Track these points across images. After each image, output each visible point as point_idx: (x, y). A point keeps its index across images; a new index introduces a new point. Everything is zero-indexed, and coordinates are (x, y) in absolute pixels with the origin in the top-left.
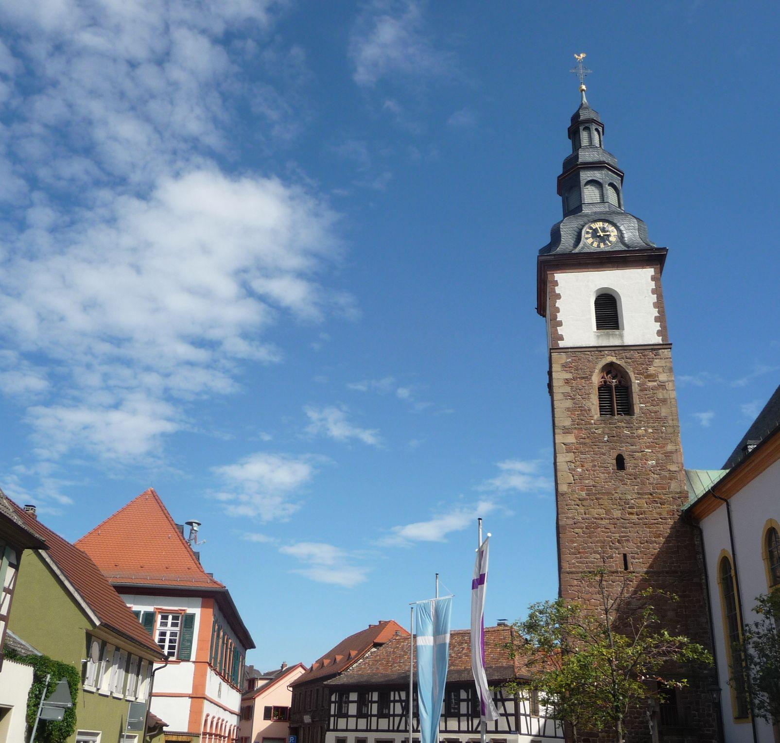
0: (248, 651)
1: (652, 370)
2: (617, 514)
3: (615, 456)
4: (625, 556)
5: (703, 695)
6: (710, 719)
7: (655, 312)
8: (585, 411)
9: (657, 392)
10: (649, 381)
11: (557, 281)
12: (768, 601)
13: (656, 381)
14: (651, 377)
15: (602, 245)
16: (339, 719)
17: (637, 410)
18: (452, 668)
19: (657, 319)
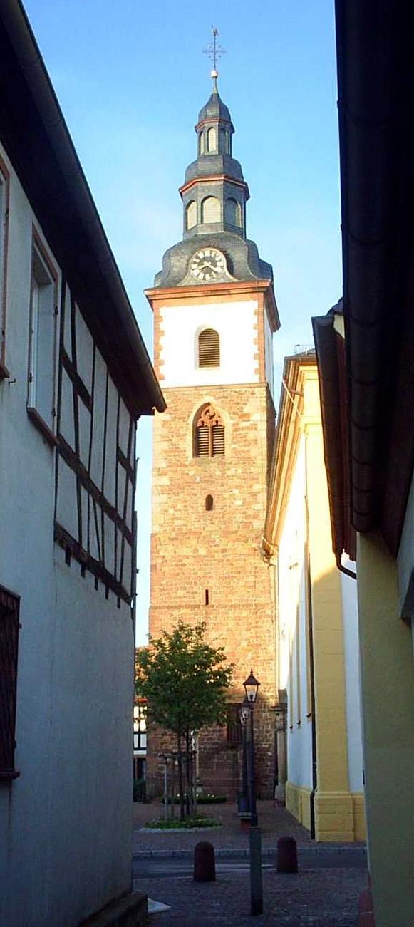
0: (144, 421)
1: (246, 410)
2: (202, 552)
3: (206, 496)
4: (207, 591)
5: (264, 714)
6: (268, 734)
7: (256, 364)
8: (179, 452)
9: (249, 432)
10: (243, 421)
11: (162, 317)
12: (219, 154)
13: (249, 421)
14: (245, 417)
15: (207, 276)
16: (262, 294)
17: (228, 451)
18: (267, 284)
19: (256, 357)
